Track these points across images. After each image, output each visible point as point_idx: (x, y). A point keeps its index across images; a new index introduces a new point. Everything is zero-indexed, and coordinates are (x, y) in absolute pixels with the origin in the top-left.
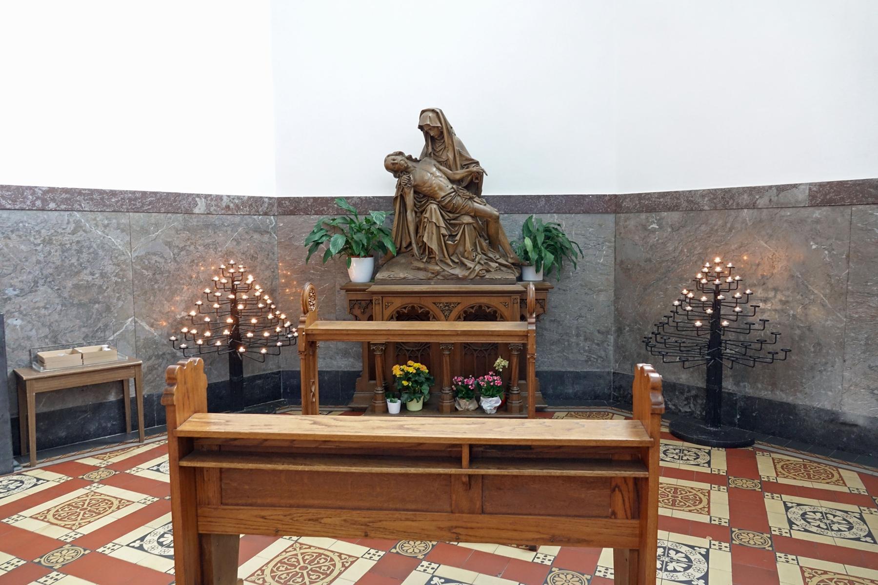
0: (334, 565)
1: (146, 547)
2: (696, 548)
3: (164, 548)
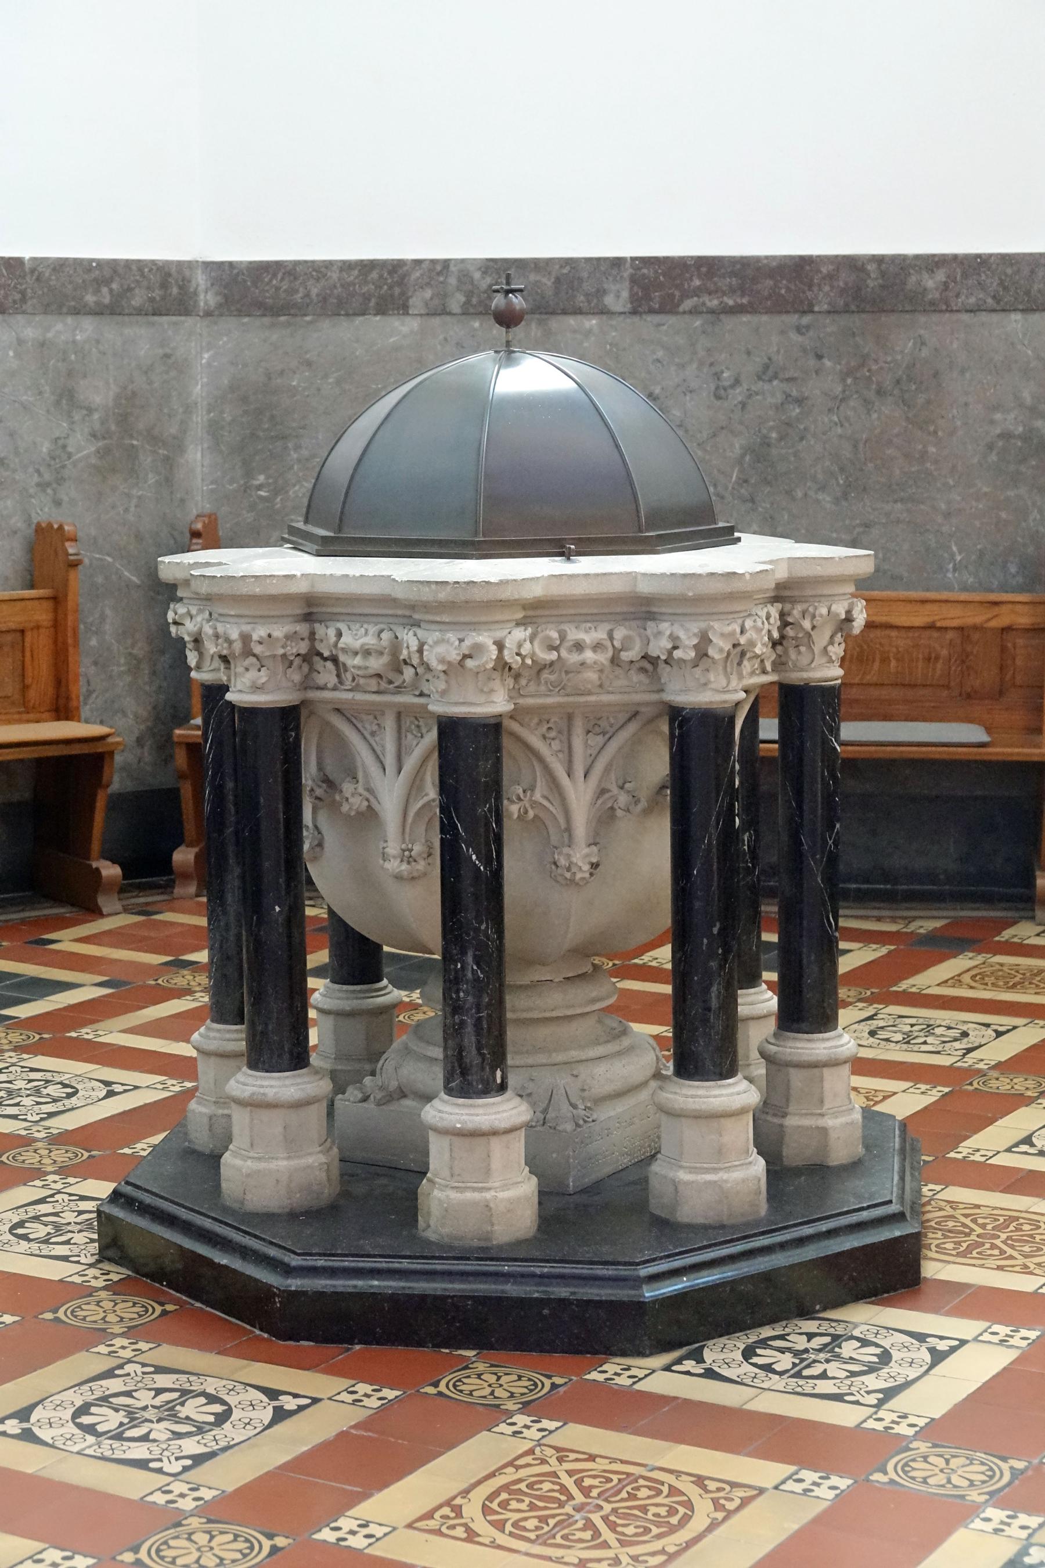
0: (486, 1510)
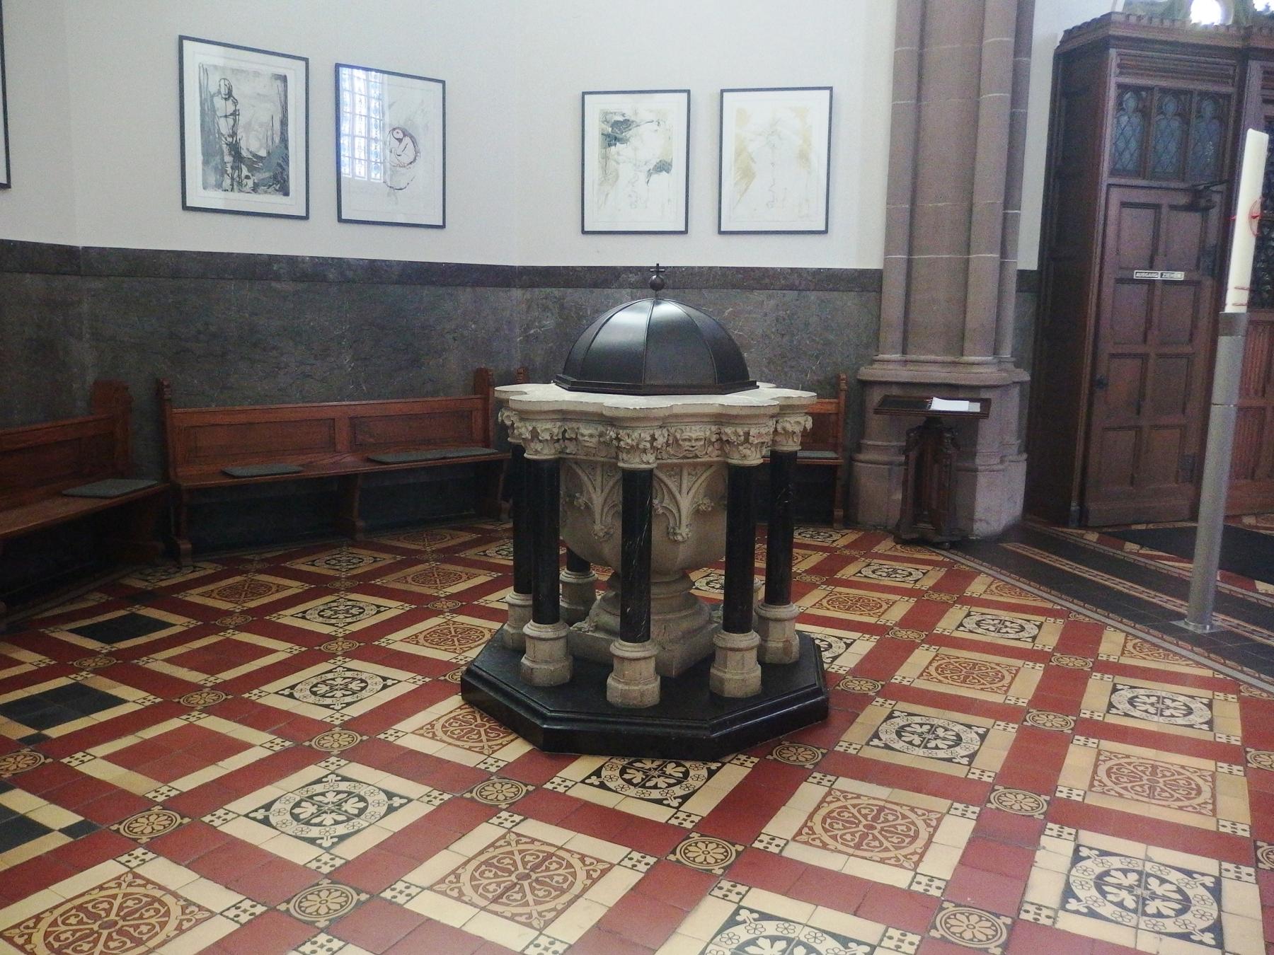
1: (273, 820)
2: (1195, 875)
3: (318, 698)
